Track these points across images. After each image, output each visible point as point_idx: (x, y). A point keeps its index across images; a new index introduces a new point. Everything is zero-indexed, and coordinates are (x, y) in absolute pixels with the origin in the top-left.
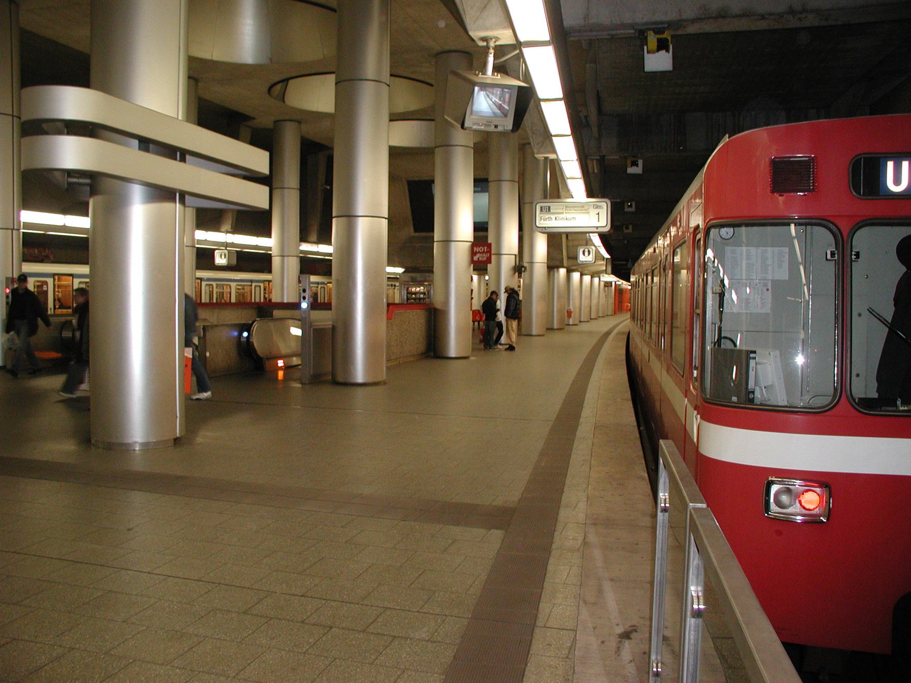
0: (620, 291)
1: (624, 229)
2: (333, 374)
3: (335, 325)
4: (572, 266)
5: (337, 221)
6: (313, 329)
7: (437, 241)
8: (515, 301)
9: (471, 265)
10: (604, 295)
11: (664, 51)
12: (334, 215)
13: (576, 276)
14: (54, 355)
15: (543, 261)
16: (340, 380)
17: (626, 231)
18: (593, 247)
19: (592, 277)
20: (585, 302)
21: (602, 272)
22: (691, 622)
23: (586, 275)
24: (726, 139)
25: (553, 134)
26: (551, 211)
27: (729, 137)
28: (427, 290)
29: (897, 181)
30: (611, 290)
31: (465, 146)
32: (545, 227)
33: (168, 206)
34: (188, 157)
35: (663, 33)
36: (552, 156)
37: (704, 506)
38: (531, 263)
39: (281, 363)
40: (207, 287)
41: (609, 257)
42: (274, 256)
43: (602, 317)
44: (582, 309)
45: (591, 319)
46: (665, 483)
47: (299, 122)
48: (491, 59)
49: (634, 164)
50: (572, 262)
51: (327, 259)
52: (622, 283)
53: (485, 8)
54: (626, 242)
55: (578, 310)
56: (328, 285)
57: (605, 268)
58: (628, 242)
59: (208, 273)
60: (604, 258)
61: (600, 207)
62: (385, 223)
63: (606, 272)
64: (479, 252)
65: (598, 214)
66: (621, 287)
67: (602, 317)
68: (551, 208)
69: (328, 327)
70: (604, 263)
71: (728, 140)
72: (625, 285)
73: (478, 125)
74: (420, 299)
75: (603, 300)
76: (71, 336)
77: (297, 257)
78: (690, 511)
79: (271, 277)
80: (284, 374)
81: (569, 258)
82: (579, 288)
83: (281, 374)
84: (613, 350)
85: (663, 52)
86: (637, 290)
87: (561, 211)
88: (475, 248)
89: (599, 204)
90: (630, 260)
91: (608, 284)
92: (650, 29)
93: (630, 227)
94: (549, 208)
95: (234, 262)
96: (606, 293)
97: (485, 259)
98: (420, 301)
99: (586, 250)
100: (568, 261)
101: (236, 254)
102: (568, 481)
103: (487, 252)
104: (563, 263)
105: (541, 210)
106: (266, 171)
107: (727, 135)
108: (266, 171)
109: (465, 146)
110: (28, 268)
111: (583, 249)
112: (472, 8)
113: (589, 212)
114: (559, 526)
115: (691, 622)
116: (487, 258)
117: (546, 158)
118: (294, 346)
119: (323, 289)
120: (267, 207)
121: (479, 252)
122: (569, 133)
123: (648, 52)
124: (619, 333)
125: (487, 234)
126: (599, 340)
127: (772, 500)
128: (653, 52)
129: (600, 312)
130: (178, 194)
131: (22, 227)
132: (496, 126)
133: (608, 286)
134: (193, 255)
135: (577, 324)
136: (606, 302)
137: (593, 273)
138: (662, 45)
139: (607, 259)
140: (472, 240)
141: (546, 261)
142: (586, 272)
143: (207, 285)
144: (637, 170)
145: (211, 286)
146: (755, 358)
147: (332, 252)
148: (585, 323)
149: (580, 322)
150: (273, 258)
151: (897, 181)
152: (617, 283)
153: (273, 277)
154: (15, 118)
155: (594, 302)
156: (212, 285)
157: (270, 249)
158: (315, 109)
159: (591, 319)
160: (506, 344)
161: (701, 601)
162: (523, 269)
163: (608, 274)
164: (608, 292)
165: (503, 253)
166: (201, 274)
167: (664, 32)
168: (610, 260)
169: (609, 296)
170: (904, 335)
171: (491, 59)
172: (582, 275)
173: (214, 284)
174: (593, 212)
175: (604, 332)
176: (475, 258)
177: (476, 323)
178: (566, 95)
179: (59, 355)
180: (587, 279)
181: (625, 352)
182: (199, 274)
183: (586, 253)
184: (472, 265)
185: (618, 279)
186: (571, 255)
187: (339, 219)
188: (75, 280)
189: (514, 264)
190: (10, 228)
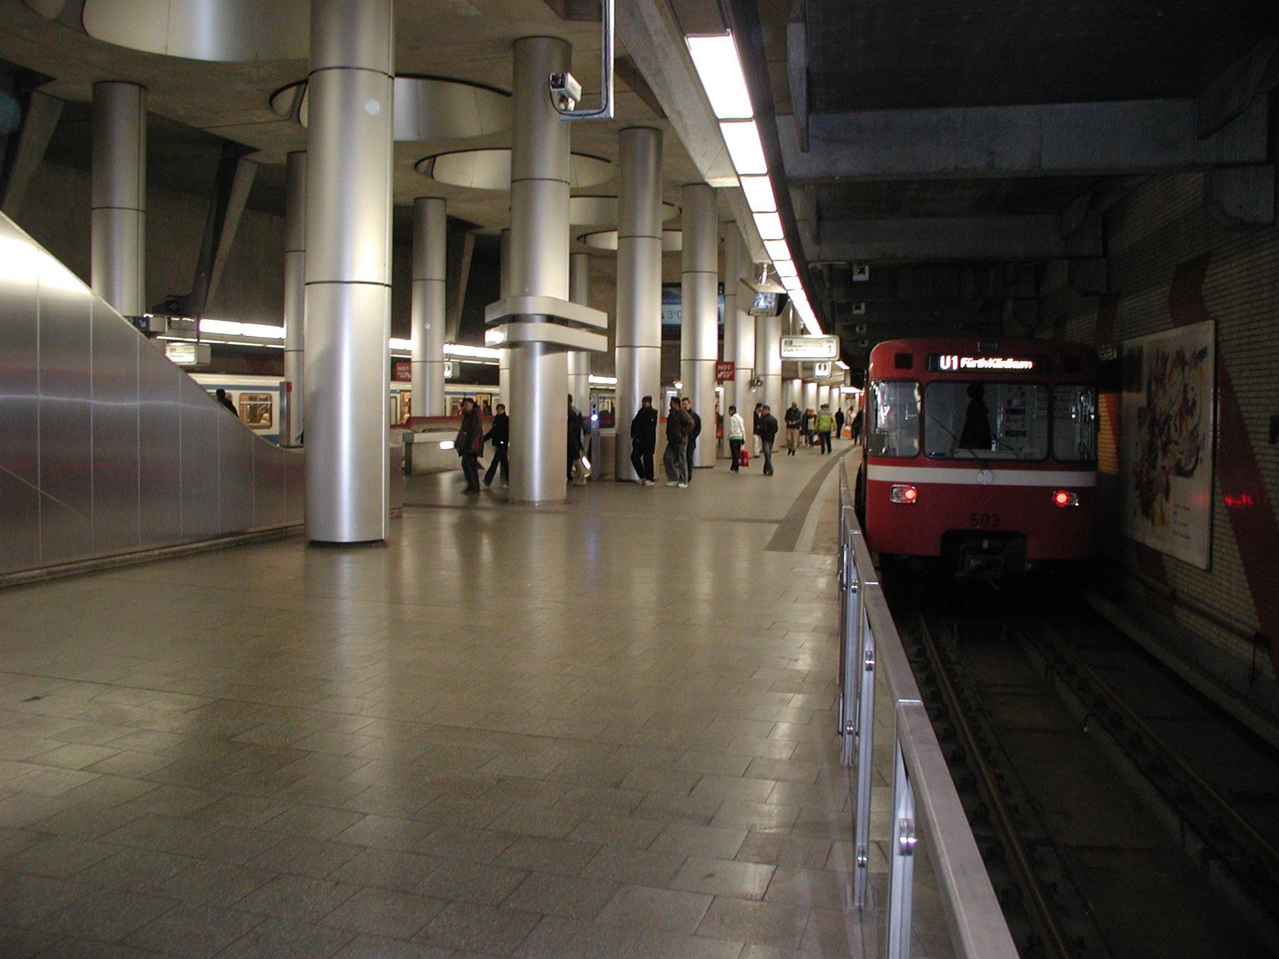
5: (620, 351)
12: (617, 345)
13: (812, 387)
25: (754, 211)
26: (793, 344)
38: (765, 375)
41: (848, 368)
48: (765, 274)
49: (859, 308)
50: (807, 373)
57: (843, 379)
59: (256, 379)
61: (831, 342)
62: (659, 351)
63: (844, 382)
64: (723, 370)
65: (830, 347)
70: (843, 373)
79: (410, 386)
85: (862, 275)
87: (801, 344)
88: (719, 367)
95: (458, 374)
97: (728, 376)
101: (459, 366)
103: (730, 370)
104: (797, 376)
106: (605, 326)
121: (723, 370)
122: (749, 112)
138: (862, 271)
141: (780, 373)
142: (822, 383)
147: (284, 336)
150: (501, 371)
153: (413, 387)
157: (409, 352)
165: (770, 373)
166: (396, 386)
168: (849, 371)
171: (765, 274)
174: (826, 345)
176: (720, 376)
180: (824, 390)
183: (823, 368)
187: (622, 348)
189: (750, 378)
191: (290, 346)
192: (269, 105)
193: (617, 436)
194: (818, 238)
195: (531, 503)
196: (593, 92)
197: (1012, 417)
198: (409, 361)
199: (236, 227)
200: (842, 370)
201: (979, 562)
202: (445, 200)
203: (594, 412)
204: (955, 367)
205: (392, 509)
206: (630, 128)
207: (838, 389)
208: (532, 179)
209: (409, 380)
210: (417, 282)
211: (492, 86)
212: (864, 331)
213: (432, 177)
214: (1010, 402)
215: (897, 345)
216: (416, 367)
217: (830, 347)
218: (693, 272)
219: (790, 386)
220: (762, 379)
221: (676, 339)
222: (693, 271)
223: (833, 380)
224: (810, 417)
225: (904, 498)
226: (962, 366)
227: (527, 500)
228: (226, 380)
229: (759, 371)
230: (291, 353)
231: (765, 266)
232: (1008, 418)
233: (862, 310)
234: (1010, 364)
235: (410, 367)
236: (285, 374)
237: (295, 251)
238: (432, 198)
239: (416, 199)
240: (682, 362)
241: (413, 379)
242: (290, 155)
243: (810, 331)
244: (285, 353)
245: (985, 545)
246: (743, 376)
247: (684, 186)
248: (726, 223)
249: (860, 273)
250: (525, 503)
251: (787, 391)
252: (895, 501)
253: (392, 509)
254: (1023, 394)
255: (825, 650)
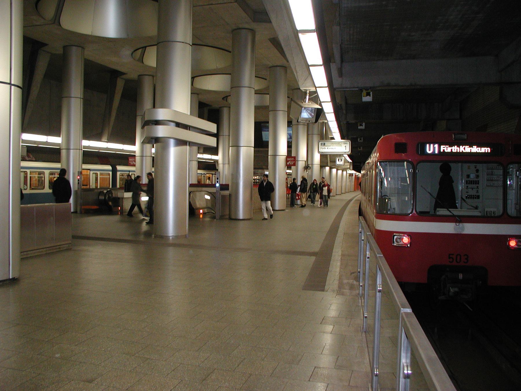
0: (357, 178)
1: (358, 149)
2: (230, 215)
3: (230, 193)
4: (333, 166)
6: (221, 196)
7: (270, 155)
8: (304, 184)
9: (286, 167)
10: (349, 181)
11: (369, 96)
14: (96, 207)
15: (318, 164)
16: (233, 217)
17: (359, 149)
18: (343, 158)
19: (342, 171)
20: (339, 184)
21: (348, 168)
22: (378, 294)
23: (339, 170)
24: (383, 137)
26: (326, 145)
27: (384, 136)
28: (260, 178)
29: (430, 150)
30: (353, 178)
31: (283, 111)
32: (323, 152)
33: (184, 147)
34: (191, 128)
35: (368, 90)
36: (326, 121)
37: (382, 255)
38: (312, 164)
39: (201, 211)
40: (94, 175)
41: (351, 161)
42: (137, 156)
43: (348, 192)
44: (337, 188)
45: (342, 193)
46: (380, 278)
47: (198, 94)
48: (308, 97)
49: (361, 125)
50: (332, 164)
51: (207, 162)
52: (359, 174)
53: (306, 79)
54: (360, 154)
55: (335, 189)
56: (207, 175)
57: (349, 167)
58: (361, 154)
60: (349, 162)
61: (347, 143)
62: (253, 149)
63: (350, 168)
64: (290, 161)
65: (346, 146)
66: (358, 176)
67: (348, 192)
68: (325, 144)
69: (227, 194)
71: (383, 137)
72: (360, 175)
73: (303, 121)
74: (257, 182)
75: (348, 183)
76: (104, 198)
77: (197, 161)
78: (402, 314)
79: (135, 168)
80: (203, 216)
81: (331, 162)
82: (336, 176)
83: (201, 216)
84: (353, 207)
85: (368, 97)
86: (367, 177)
87: (330, 145)
88: (288, 159)
89: (346, 142)
90: (362, 163)
91: (351, 175)
92: (364, 89)
93: (361, 148)
94: (325, 143)
96: (350, 180)
97: (293, 164)
98: (257, 183)
99: (340, 159)
100: (330, 163)
102: (334, 247)
104: (328, 165)
105: (321, 145)
106: (215, 132)
107: (383, 135)
108: (215, 132)
109: (283, 111)
110: (85, 166)
111: (338, 159)
112: (301, 79)
113: (341, 146)
114: (333, 256)
115: (378, 294)
116: (294, 163)
117: (323, 122)
118: (204, 205)
119: (204, 177)
120: (216, 146)
123: (363, 96)
124: (356, 200)
125: (292, 149)
126: (346, 203)
127: (395, 241)
128: (365, 96)
129: (347, 190)
130: (188, 143)
131: (83, 148)
132: (309, 121)
133: (351, 176)
134: (151, 160)
135: (334, 195)
136: (350, 184)
137: (343, 169)
138: (368, 94)
139: (350, 162)
140: (287, 155)
141: (320, 164)
142: (339, 169)
143: (93, 173)
144: (363, 127)
145: (96, 174)
146: (390, 200)
148: (338, 195)
149: (336, 195)
151: (430, 150)
152: (356, 174)
154: (81, 99)
155: (344, 184)
156: (97, 173)
157: (135, 152)
158: (207, 89)
159: (342, 193)
160: (300, 205)
161: (409, 368)
162: (309, 168)
163: (351, 170)
164: (351, 179)
167: (369, 90)
169: (396, 179)
170: (97, 150)
171: (308, 97)
172: (337, 170)
173: (99, 173)
174: (344, 146)
175: (348, 200)
176: (288, 164)
177: (288, 195)
178: (333, 99)
179: (98, 207)
180: (340, 172)
181: (358, 208)
182: (84, 166)
183: (340, 160)
184: (286, 167)
185: (356, 172)
186: (332, 160)
187: (232, 147)
188: (91, 172)
189: (304, 165)
190: (78, 148)
191: (64, 146)
192: (36, 9)
193: (230, 195)
194: (341, 75)
195: (167, 237)
196: (214, 3)
197: (470, 186)
198: (135, 156)
199: (39, 85)
200: (348, 162)
201: (456, 289)
202: (153, 76)
203: (217, 182)
204: (436, 152)
205: (21, 252)
206: (238, 29)
207: (346, 172)
208: (169, 41)
209: (134, 165)
210: (138, 116)
211: (196, 45)
212: (362, 141)
213: (143, 63)
214: (468, 176)
215: (394, 137)
216: (138, 159)
217: (346, 146)
218: (274, 111)
219: (324, 170)
220: (310, 166)
221: (267, 148)
222: (275, 110)
223: (344, 167)
224: (324, 186)
225: (401, 243)
226: (442, 151)
227: (166, 235)
228: (43, 165)
229: (309, 163)
230: (64, 150)
231: (308, 92)
232: (467, 187)
233: (363, 127)
234: (475, 149)
235: (135, 159)
236: (61, 162)
237: (66, 97)
238: (146, 75)
239: (139, 76)
240: (269, 156)
241: (136, 165)
242: (65, 47)
243: (335, 139)
244: (61, 150)
245: (461, 276)
246: (301, 164)
247: (270, 67)
248: (293, 90)
249: (367, 95)
250: (162, 237)
251: (323, 172)
252: (395, 245)
253: (21, 252)
254: (477, 171)
255: (337, 289)
